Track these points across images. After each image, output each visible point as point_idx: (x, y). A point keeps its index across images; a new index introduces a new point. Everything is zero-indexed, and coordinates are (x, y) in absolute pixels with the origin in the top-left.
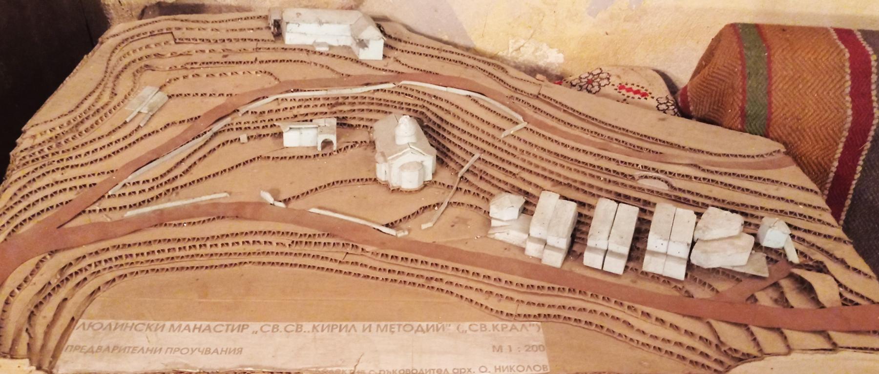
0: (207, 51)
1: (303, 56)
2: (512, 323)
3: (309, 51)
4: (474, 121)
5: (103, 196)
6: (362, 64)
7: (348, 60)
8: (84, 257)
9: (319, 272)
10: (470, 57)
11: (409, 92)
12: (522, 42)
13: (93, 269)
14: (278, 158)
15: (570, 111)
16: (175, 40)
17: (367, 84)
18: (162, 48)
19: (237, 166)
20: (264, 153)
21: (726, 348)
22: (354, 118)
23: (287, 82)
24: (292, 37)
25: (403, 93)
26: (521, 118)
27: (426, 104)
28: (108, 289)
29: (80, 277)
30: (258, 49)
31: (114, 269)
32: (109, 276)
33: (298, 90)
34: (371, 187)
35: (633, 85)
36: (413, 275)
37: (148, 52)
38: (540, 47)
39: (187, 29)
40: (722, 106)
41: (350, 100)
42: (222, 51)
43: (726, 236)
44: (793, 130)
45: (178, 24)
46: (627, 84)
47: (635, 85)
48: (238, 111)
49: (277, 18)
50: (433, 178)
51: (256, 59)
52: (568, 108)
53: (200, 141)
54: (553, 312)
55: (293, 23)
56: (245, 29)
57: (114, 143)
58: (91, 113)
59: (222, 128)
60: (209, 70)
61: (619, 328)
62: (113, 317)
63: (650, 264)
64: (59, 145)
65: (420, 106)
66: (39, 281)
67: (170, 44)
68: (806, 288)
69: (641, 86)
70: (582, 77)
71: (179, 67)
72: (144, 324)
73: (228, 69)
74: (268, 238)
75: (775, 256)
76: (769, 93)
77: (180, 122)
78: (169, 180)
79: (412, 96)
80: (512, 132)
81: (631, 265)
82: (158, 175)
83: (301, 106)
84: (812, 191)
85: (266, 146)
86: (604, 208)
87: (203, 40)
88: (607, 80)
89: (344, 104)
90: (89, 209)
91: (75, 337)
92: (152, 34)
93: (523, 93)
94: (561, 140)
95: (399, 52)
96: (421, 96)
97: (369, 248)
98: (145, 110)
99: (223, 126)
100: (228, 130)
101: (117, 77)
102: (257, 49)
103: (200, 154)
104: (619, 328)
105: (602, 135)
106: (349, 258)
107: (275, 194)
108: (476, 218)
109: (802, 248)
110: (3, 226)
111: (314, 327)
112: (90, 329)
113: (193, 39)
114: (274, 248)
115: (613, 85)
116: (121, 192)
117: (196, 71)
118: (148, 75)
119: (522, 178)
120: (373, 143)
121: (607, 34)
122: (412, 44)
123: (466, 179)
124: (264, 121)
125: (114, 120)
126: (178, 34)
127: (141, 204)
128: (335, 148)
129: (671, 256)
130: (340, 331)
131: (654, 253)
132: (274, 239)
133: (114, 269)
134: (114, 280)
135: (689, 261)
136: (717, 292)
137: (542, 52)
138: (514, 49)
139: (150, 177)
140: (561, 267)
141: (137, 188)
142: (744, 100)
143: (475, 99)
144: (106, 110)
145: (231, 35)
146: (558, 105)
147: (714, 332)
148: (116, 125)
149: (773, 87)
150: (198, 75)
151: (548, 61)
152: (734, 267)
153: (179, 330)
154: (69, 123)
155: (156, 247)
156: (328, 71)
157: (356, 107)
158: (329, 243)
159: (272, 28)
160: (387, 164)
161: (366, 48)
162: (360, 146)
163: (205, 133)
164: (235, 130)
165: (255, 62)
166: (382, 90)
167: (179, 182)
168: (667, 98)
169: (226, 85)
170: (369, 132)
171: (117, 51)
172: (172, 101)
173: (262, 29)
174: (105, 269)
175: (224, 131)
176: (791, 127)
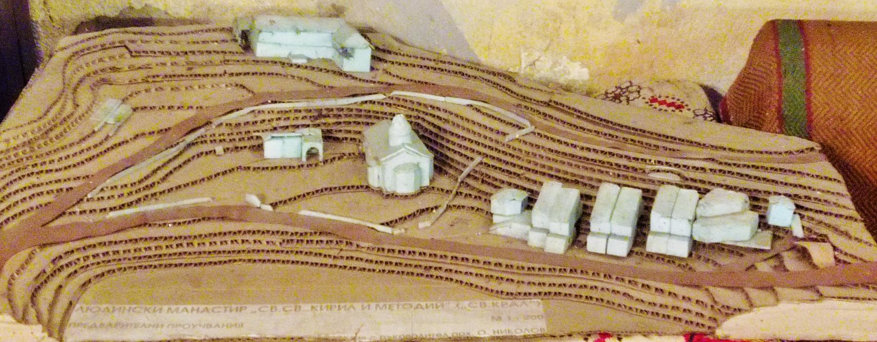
0: (169, 64)
1: (278, 69)
2: (512, 301)
3: (284, 64)
4: (476, 129)
5: (82, 200)
6: (347, 76)
7: (330, 72)
8: (72, 251)
9: (314, 268)
10: (472, 68)
11: (401, 103)
12: (536, 55)
13: (82, 263)
14: (259, 168)
15: (585, 116)
16: (131, 52)
17: (354, 96)
18: (118, 62)
19: (216, 176)
20: (244, 164)
21: (719, 307)
22: (340, 131)
23: (262, 95)
24: (264, 48)
25: (395, 105)
26: (528, 123)
27: (422, 115)
28: (98, 282)
29: (71, 270)
30: (226, 62)
31: (102, 264)
32: (99, 271)
33: (276, 102)
34: (362, 195)
35: (667, 97)
36: (410, 265)
37: (101, 66)
38: (559, 61)
39: (142, 41)
40: (762, 112)
41: (335, 112)
42: (185, 64)
43: (728, 213)
44: (838, 132)
45: (133, 37)
46: (660, 97)
47: (670, 98)
48: (211, 123)
49: (245, 27)
50: (431, 184)
51: (225, 73)
52: (582, 113)
53: (174, 151)
54: (553, 290)
55: (266, 32)
56: (208, 42)
57: (28, 199)
58: (58, 121)
59: (196, 139)
60: (174, 84)
61: (618, 299)
62: (110, 303)
63: (654, 245)
64: (32, 150)
65: (415, 117)
66: (34, 268)
67: (126, 58)
68: (804, 254)
69: (677, 97)
70: (608, 91)
71: (140, 81)
72: (141, 308)
73: (196, 83)
74: (257, 237)
75: (779, 234)
76: (808, 92)
77: (150, 133)
78: (147, 186)
79: (405, 107)
80: (517, 136)
81: (636, 249)
82: (136, 180)
83: (279, 119)
84: (835, 180)
85: (246, 158)
86: (607, 192)
87: (163, 53)
88: (637, 93)
89: (329, 116)
90: (69, 211)
91: (75, 316)
92: (104, 48)
93: (532, 101)
94: (570, 141)
95: (389, 64)
96: (415, 107)
97: (362, 244)
98: (111, 121)
99: (196, 137)
100: (202, 142)
101: (75, 90)
102: (224, 61)
103: (176, 163)
104: (618, 299)
105: (617, 137)
106: (344, 254)
107: (262, 198)
108: (477, 219)
109: (807, 224)
110: (3, 211)
111: (313, 307)
112: (89, 311)
113: (151, 52)
114: (264, 246)
115: (644, 98)
116: (100, 195)
117: (158, 85)
118: (105, 89)
119: (526, 178)
120: (362, 156)
121: (639, 42)
122: (404, 55)
123: (466, 183)
124: (241, 133)
125: (83, 129)
126: (132, 47)
127: (122, 207)
128: (321, 158)
129: (675, 235)
130: (339, 309)
131: (657, 234)
132: (264, 238)
133: (102, 264)
134: (103, 274)
135: (691, 237)
136: (720, 265)
137: (561, 68)
138: (528, 64)
139: (128, 181)
140: (565, 253)
141: (116, 193)
142: (780, 101)
143: (477, 107)
144: (72, 119)
145: (195, 47)
146: (571, 111)
147: (711, 295)
148: (85, 134)
149: (813, 85)
150: (161, 89)
151: (571, 77)
152: (737, 242)
153: (177, 312)
154: (40, 129)
155: (141, 245)
156: (309, 84)
157: (342, 120)
158: (321, 241)
159: (239, 39)
160: (380, 168)
161: (351, 58)
162: (348, 158)
163: (178, 143)
164: (209, 142)
165: (224, 75)
166: (371, 102)
167: (157, 189)
168: (706, 110)
169: (194, 97)
170: (358, 145)
171: (69, 64)
172: (137, 115)
173: (227, 41)
174: (93, 264)
175: (197, 143)
176: (835, 129)
